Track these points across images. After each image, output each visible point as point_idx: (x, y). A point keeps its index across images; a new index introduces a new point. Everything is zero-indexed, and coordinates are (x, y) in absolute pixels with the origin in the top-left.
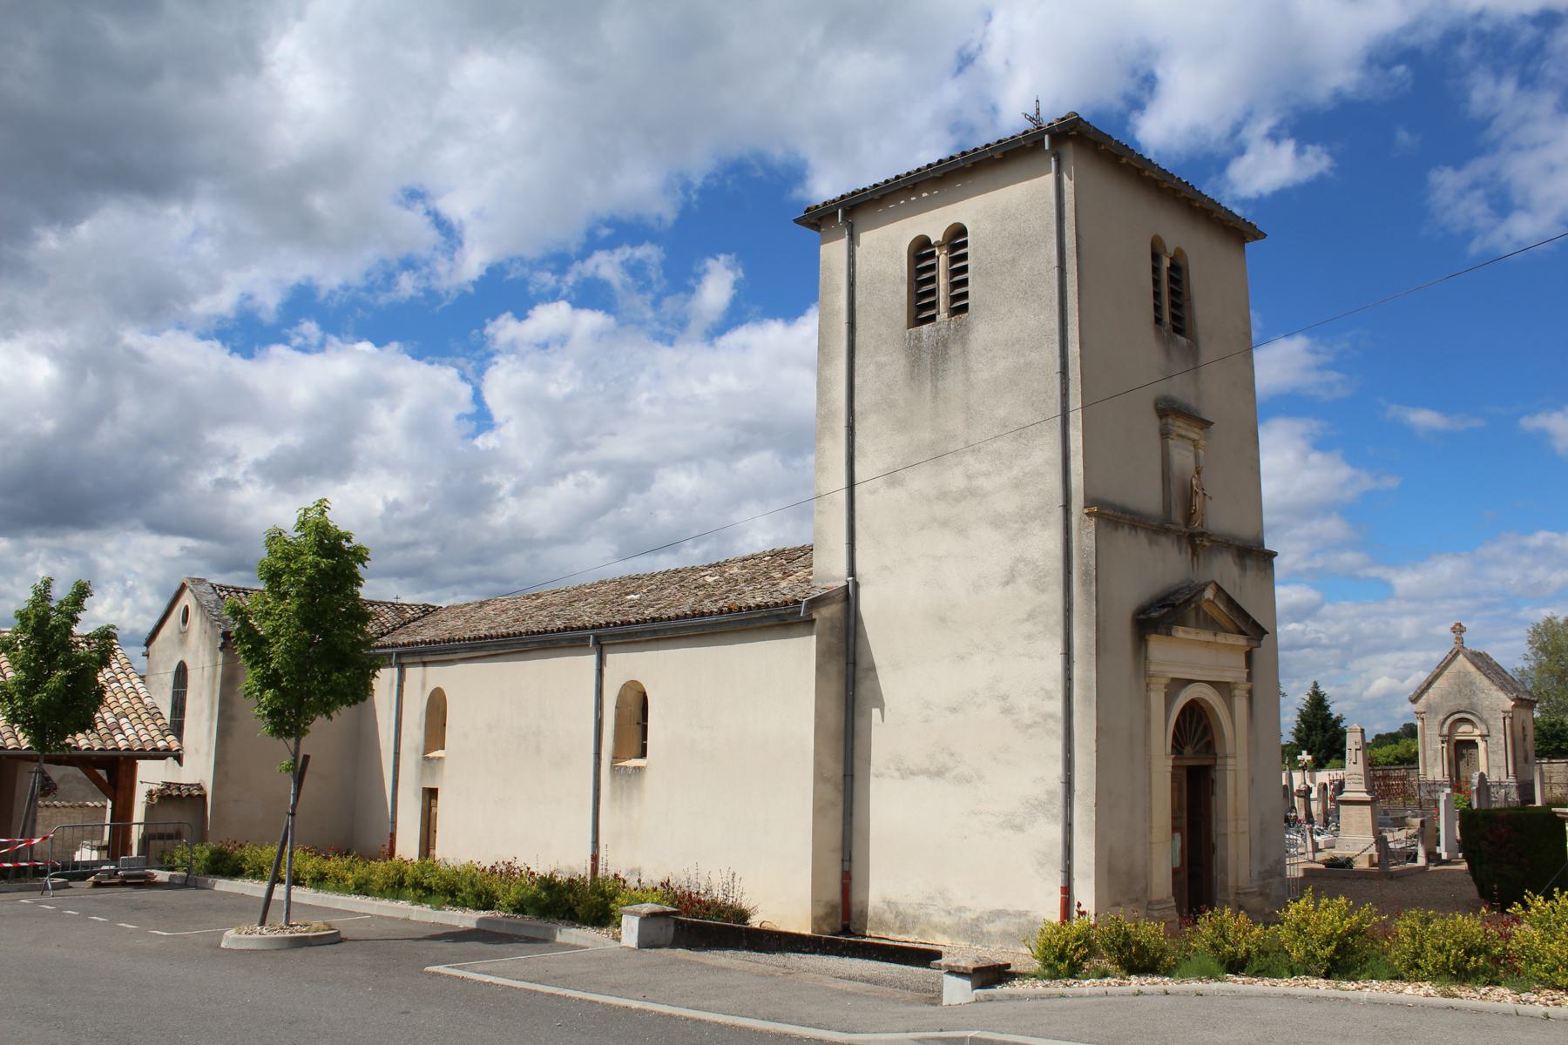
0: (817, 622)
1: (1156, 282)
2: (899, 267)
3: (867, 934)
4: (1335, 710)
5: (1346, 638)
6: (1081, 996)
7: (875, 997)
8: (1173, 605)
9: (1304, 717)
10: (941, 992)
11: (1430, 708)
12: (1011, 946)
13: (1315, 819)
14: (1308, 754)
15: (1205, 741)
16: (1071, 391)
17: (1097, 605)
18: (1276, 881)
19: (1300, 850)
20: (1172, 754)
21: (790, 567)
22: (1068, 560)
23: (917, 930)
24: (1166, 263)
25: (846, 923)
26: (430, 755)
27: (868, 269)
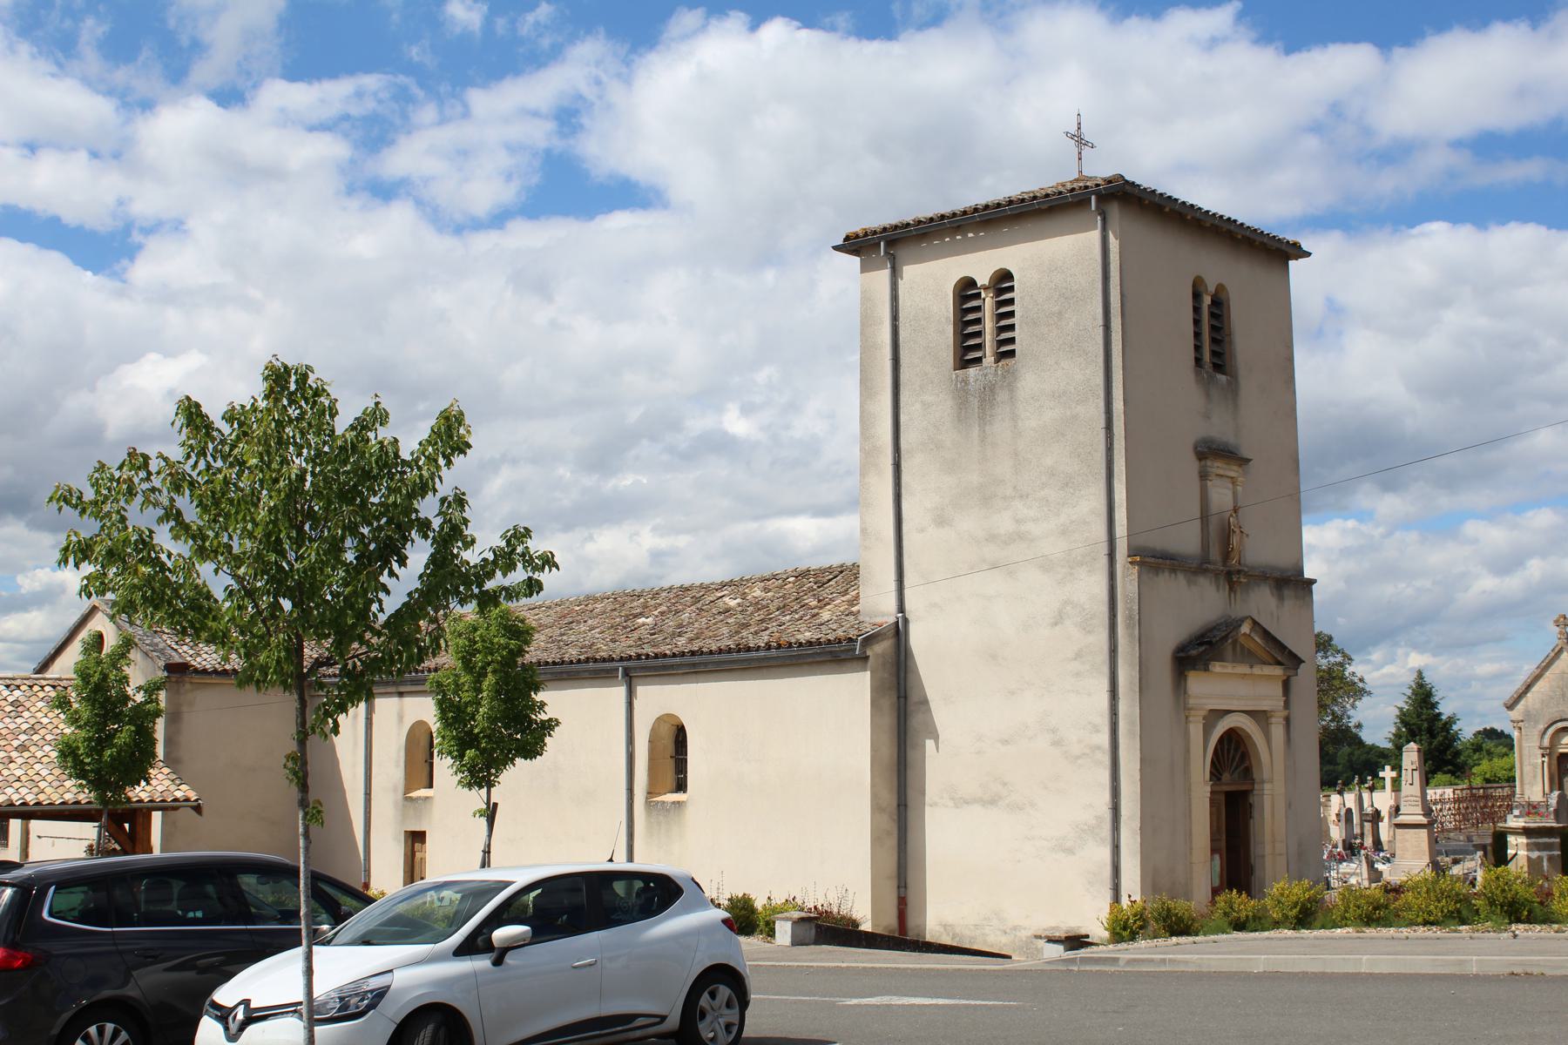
1: (1197, 322)
2: (945, 308)
4: (1445, 709)
8: (1210, 643)
11: (1529, 716)
15: (1242, 767)
20: (1211, 780)
22: (1113, 604)
26: (414, 794)
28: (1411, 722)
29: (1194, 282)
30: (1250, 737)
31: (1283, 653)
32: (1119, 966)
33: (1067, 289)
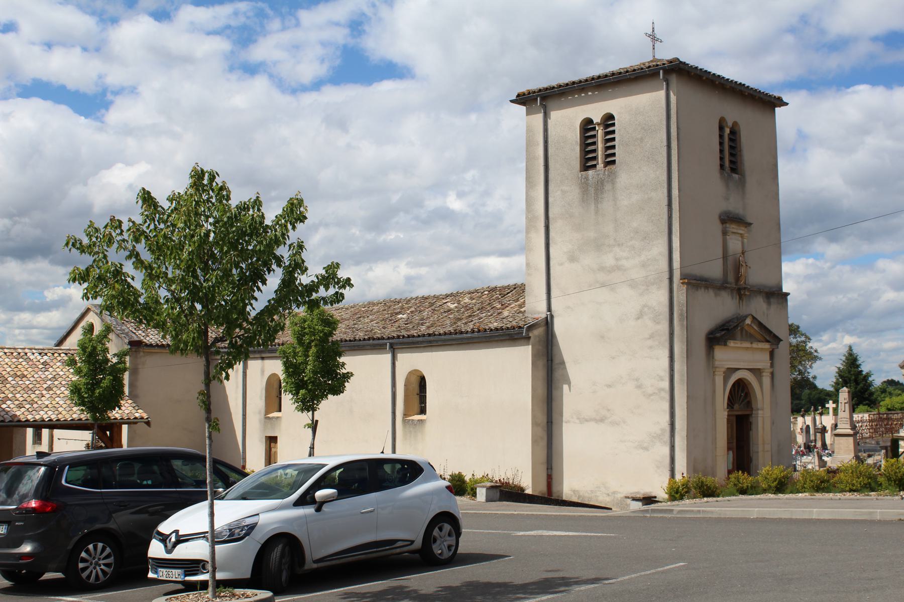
0: (532, 338)
1: (721, 144)
2: (575, 135)
4: (865, 368)
8: (728, 329)
14: (828, 403)
15: (746, 401)
16: (674, 215)
17: (687, 332)
22: (672, 307)
26: (271, 415)
27: (556, 134)
28: (845, 376)
30: (750, 384)
32: (673, 514)
33: (645, 124)
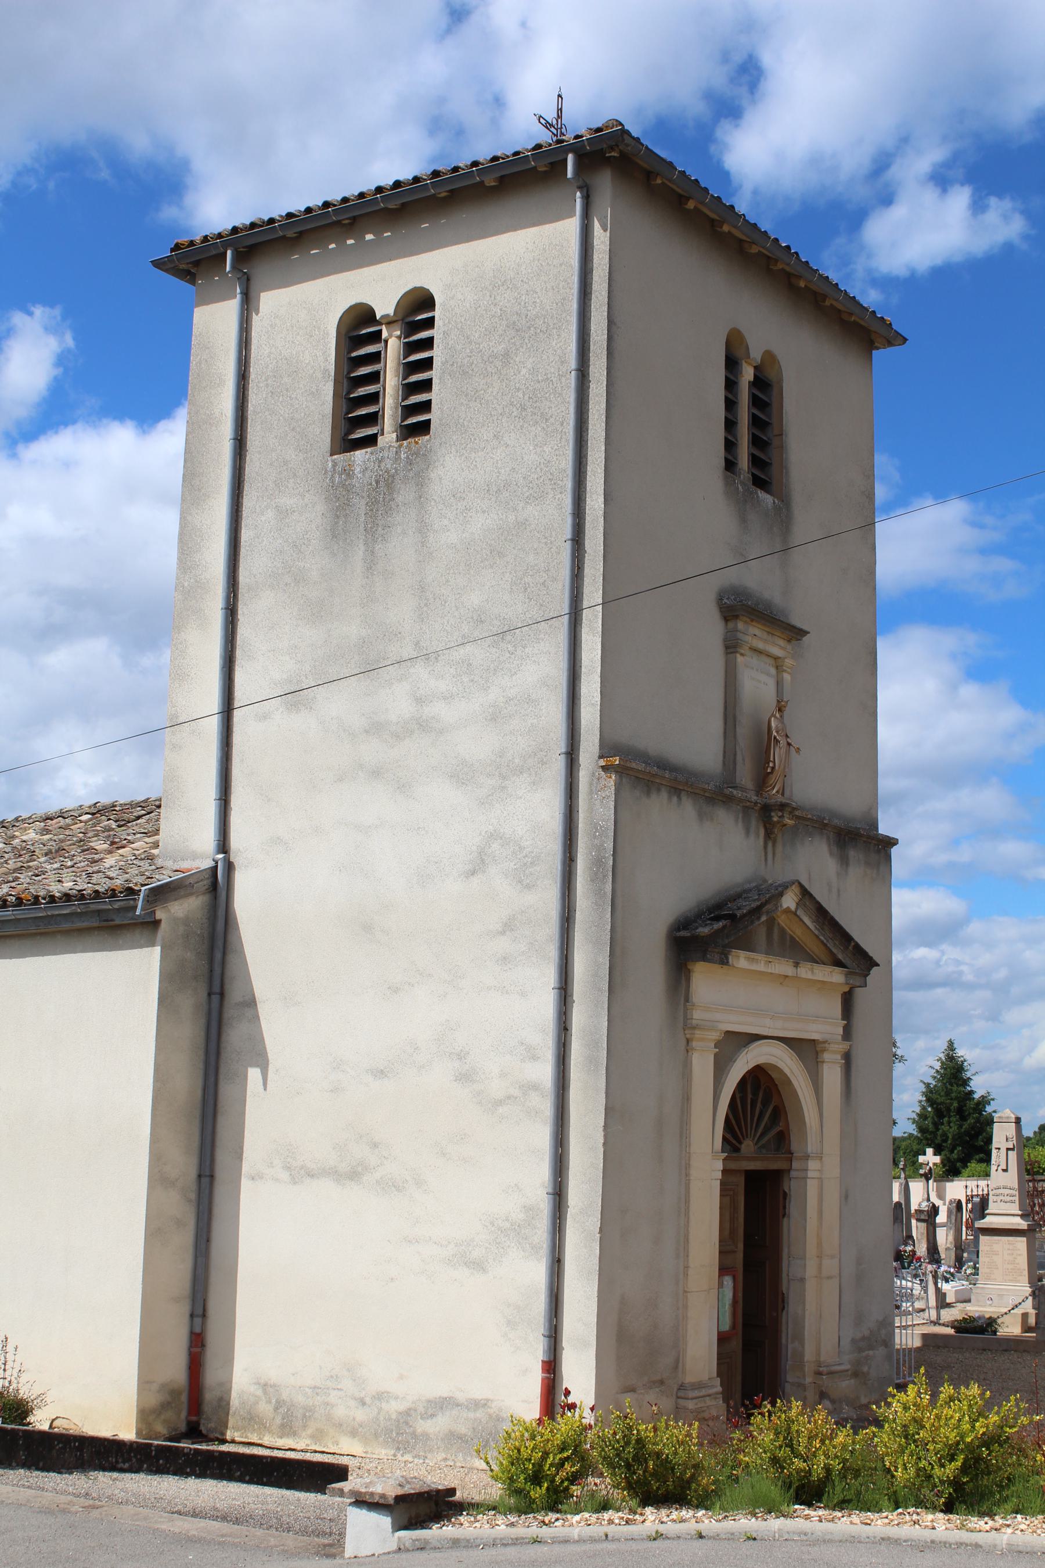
0: (163, 925)
1: (730, 404)
3: (228, 1437)
4: (979, 1086)
5: (1002, 974)
6: (566, 1541)
7: (235, 1545)
8: (732, 917)
9: (930, 1095)
10: (342, 1534)
12: (460, 1456)
13: (943, 1256)
14: (935, 1154)
18: (880, 1352)
19: (918, 1305)
20: (723, 1152)
21: (122, 833)
23: (309, 1431)
24: (748, 374)
25: (194, 1418)
28: (939, 1101)
29: (727, 343)
30: (789, 1082)
31: (847, 948)
